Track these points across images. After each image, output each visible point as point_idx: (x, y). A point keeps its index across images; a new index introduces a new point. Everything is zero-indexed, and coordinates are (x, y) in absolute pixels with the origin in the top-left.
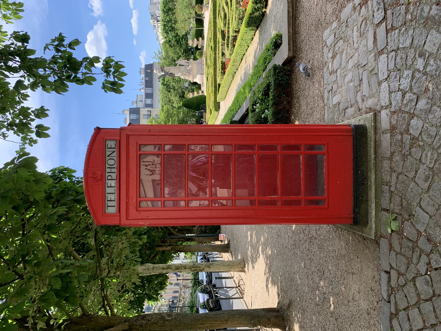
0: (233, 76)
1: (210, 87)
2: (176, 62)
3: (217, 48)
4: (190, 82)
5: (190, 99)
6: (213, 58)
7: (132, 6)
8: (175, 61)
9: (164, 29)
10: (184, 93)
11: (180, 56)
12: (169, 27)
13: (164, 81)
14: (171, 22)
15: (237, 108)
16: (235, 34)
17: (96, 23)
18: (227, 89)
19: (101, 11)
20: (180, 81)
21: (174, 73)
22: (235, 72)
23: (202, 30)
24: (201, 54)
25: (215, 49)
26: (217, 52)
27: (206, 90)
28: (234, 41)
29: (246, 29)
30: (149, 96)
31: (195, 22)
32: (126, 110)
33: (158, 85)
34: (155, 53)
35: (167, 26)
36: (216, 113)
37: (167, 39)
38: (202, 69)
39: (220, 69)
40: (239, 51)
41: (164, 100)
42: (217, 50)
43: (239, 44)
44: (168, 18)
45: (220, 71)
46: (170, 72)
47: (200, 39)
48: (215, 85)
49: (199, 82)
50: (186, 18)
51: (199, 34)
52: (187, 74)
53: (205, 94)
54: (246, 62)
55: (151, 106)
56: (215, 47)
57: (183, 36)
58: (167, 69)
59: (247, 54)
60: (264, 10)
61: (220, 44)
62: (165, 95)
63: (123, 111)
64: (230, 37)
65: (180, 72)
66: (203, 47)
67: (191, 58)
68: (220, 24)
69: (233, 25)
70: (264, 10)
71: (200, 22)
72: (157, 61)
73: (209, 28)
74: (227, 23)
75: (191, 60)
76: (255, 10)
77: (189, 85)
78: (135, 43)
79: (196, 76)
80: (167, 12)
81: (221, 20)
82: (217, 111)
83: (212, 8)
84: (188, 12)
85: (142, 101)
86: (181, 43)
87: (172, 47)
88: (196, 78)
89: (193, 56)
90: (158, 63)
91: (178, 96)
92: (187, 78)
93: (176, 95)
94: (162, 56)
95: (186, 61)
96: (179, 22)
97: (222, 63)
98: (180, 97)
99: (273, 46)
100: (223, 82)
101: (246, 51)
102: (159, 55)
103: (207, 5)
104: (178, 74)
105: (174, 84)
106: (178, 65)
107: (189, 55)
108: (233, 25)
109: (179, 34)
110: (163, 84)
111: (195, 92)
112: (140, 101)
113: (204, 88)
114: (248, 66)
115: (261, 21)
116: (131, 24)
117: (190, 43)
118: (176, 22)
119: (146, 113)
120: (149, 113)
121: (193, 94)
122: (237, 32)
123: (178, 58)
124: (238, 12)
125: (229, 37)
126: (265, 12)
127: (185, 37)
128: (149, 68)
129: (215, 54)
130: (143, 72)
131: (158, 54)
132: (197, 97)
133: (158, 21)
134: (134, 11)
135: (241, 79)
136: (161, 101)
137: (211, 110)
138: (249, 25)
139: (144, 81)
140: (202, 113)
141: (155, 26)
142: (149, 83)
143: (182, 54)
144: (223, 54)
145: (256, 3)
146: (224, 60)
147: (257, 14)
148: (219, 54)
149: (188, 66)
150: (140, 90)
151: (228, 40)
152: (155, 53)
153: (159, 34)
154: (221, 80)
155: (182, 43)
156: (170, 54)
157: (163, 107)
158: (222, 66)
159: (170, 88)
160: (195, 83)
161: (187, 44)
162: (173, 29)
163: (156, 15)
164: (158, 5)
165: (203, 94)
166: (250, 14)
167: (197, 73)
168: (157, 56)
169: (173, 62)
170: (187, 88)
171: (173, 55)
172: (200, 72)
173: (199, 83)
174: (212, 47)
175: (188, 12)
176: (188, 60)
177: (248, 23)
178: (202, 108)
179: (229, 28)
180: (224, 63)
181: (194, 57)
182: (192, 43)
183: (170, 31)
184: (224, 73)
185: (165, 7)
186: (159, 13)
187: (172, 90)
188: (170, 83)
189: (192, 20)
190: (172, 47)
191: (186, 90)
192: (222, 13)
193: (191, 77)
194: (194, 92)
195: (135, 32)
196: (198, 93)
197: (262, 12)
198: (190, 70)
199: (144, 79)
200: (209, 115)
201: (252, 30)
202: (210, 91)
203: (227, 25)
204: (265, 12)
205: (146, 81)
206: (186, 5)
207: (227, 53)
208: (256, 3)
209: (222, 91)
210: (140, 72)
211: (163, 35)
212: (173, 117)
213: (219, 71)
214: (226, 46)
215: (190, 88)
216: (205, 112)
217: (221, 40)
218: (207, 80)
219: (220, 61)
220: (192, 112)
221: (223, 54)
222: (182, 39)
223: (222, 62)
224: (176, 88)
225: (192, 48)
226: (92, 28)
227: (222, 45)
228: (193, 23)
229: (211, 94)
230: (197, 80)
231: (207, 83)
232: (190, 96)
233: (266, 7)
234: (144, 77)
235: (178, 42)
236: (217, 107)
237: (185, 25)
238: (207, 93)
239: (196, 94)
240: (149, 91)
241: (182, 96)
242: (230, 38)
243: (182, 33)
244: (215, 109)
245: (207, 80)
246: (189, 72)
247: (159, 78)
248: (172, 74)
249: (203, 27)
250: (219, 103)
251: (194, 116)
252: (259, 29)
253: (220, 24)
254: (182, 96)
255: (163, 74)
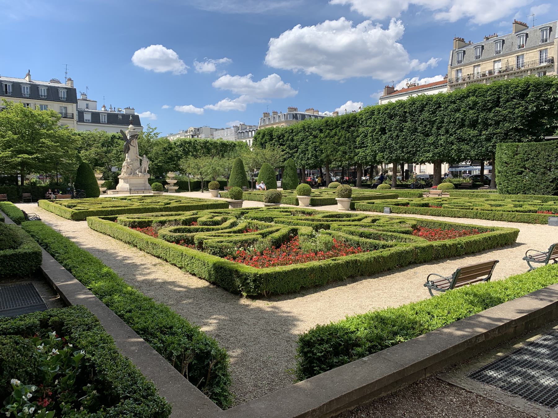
0: (129, 243)
1: (112, 204)
2: (144, 156)
3: (170, 213)
4: (119, 174)
5: (93, 174)
6: (155, 206)
7: (207, 107)
8: (146, 154)
9: (185, 142)
10: (102, 165)
11: (153, 161)
12: (190, 148)
13: (118, 139)
14: (194, 151)
15: (68, 261)
16: (196, 242)
17: (186, 63)
18: (109, 232)
19: (201, 71)
20: (119, 161)
21: (129, 152)
22: (136, 246)
23: (188, 190)
24: (157, 189)
25: (166, 209)
26: (164, 213)
27: (108, 197)
28: (184, 240)
29: (211, 265)
30: (96, 118)
31: (196, 180)
32: (72, 84)
33: (112, 131)
34: (155, 129)
35: (189, 146)
36: (69, 215)
37: (173, 146)
38: (137, 191)
39: (140, 220)
40: (172, 253)
41: (89, 136)
42: (167, 213)
43: (184, 253)
44: (198, 147)
45: (137, 220)
46: (131, 147)
47: (177, 188)
48: (114, 211)
49: (119, 187)
50: (201, 169)
51: (183, 186)
52: (129, 170)
53: (101, 196)
54: (155, 265)
55: (81, 119)
56: (170, 209)
57: (178, 165)
58: (135, 142)
59: (168, 266)
60: (244, 294)
61: (177, 218)
62: (97, 139)
63: (70, 80)
64: (192, 234)
65: (132, 160)
66: (167, 191)
67: (150, 175)
68: (204, 216)
69: (209, 238)
70: (244, 294)
71: (197, 186)
72: (145, 130)
73: (193, 200)
74: (209, 227)
75: (148, 176)
76: (244, 278)
77: (114, 173)
78: (165, 107)
79: (127, 183)
80: (205, 147)
81: (210, 216)
82: (72, 216)
83: (219, 202)
84: (208, 171)
85: (87, 108)
86: (169, 162)
87: (164, 151)
88: (124, 182)
89: (154, 178)
90: (142, 131)
91: (97, 157)
92: (124, 170)
93: (98, 154)
94: (152, 138)
95: (148, 169)
96: (196, 161)
97: (149, 221)
98: (96, 160)
99: (201, 350)
100: (120, 226)
101: (172, 264)
102: (152, 134)
103: (219, 195)
104: (128, 158)
105: (115, 152)
106: (141, 158)
107: (155, 173)
108: (209, 238)
109: (182, 160)
110: (114, 137)
111: (103, 182)
112: (87, 105)
113: (110, 194)
114: (148, 271)
115: (226, 289)
116: (188, 105)
117: (170, 174)
118: (195, 157)
119: (70, 111)
120: (69, 115)
121: (101, 179)
122: (201, 246)
123: (150, 159)
124: (230, 245)
125: (189, 231)
126: (242, 296)
127: (177, 168)
128: (136, 121)
129: (161, 210)
130: (129, 112)
131: (155, 132)
132: (96, 184)
133: (192, 136)
134: (202, 110)
135: (125, 258)
136: (88, 132)
137: (74, 206)
138: (218, 268)
139: (116, 112)
140: (71, 192)
141: (186, 132)
142: (113, 119)
143: (155, 164)
144: (162, 223)
145: (254, 281)
146: (154, 225)
147: (238, 282)
148: (162, 216)
149: (141, 172)
150: (104, 107)
151: (183, 231)
152: (155, 129)
153: (178, 136)
154: (122, 222)
155: (170, 164)
156: (155, 148)
157: (79, 135)
158: (145, 222)
159: (108, 146)
160: (117, 182)
161: (167, 171)
162: (186, 153)
163: (199, 134)
164: (211, 137)
165: (101, 193)
166: (236, 271)
167: (128, 186)
168: (151, 130)
169: (144, 151)
170: (110, 170)
171: (154, 151)
172: (132, 188)
173: (117, 187)
174: (169, 204)
175: (208, 171)
176: (148, 172)
177: (221, 268)
178: (79, 191)
179: (202, 230)
180: (149, 226)
181: (153, 179)
182: (171, 177)
183: (184, 150)
184: (133, 225)
185: (211, 144)
186: (202, 137)
187: (105, 149)
188: (116, 147)
189: (199, 177)
190: (164, 151)
191: (106, 168)
192: (219, 218)
193: (126, 175)
194: (105, 180)
195: (177, 108)
196: (103, 185)
197: (240, 291)
198: (135, 174)
199: (119, 113)
200: (66, 204)
201: (210, 274)
202: (105, 204)
203: (206, 227)
204: (242, 296)
205: (117, 115)
206: (217, 169)
207: (165, 230)
208: (254, 281)
209: (105, 225)
210: (129, 108)
211: (178, 141)
212: (62, 149)
213: (136, 217)
214: (176, 227)
215: (110, 174)
216: (73, 197)
217: (183, 218)
218: (122, 199)
219: (152, 219)
220: (73, 177)
221: (162, 223)
222: (174, 164)
223: (151, 222)
224: (109, 155)
225: (164, 177)
226: (180, 58)
227: (176, 220)
228: (197, 178)
229: (101, 206)
230: (122, 184)
231: (117, 198)
232: (98, 175)
233: (248, 297)
234: (122, 112)
235: (171, 159)
236: (78, 217)
237: (195, 167)
238: (102, 200)
239: (100, 182)
240: (103, 118)
241: (97, 163)
242: (189, 234)
243: (183, 164)
244: (75, 214)
245: (122, 199)
246: (132, 173)
247: (122, 132)
248: (129, 149)
249: (192, 191)
250: (85, 220)
251: (67, 180)
252: (212, 286)
253: (204, 216)
254: (97, 163)
255: (128, 138)
